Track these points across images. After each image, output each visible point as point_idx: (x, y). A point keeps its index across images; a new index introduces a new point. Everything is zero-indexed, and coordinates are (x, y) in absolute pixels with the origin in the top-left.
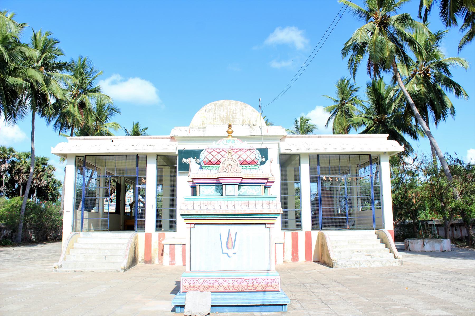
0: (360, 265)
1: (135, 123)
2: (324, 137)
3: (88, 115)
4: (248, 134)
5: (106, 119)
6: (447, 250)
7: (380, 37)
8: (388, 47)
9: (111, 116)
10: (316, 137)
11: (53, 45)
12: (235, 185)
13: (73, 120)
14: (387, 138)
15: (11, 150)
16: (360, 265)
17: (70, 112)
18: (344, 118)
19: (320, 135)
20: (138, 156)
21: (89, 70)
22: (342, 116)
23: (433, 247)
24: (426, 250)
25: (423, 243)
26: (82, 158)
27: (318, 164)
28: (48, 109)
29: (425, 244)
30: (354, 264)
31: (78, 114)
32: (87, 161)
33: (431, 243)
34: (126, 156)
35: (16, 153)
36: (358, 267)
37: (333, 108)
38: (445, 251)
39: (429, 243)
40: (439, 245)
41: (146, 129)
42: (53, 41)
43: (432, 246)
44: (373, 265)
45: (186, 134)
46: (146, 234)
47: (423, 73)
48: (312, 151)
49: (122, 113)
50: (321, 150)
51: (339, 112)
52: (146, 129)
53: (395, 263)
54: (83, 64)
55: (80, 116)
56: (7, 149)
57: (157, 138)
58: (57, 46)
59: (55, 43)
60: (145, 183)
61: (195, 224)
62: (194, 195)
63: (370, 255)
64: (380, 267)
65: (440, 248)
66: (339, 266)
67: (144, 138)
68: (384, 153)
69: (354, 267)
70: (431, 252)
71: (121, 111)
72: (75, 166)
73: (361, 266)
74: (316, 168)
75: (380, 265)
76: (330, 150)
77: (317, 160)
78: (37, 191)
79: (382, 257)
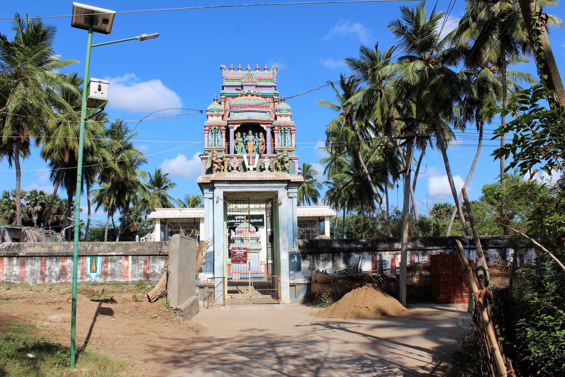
1: (157, 170)
3: (126, 171)
5: (135, 169)
7: (346, 128)
8: (351, 135)
9: (138, 166)
12: (295, 286)
13: (115, 174)
15: (42, 193)
17: (113, 168)
18: (337, 169)
21: (124, 131)
22: (335, 167)
31: (119, 169)
35: (46, 196)
37: (327, 160)
41: (167, 174)
47: (385, 145)
49: (148, 163)
51: (333, 164)
52: (167, 174)
54: (120, 125)
55: (120, 170)
56: (39, 193)
62: (290, 286)
71: (148, 161)
78: (451, 328)
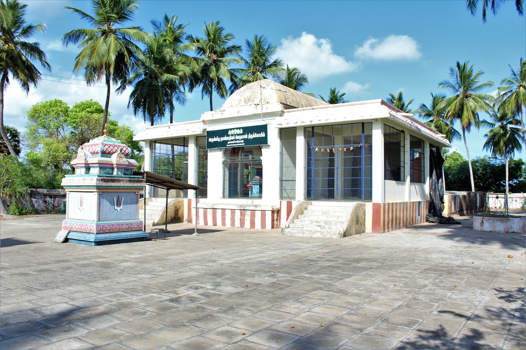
0: (303, 234)
2: (317, 108)
4: (251, 113)
6: (516, 231)
10: (310, 109)
11: (220, 33)
14: (380, 103)
16: (303, 234)
19: (313, 107)
20: (363, 123)
23: (493, 227)
24: (485, 230)
25: (482, 221)
26: (311, 129)
27: (363, 132)
28: (222, 91)
29: (484, 222)
30: (298, 233)
32: (315, 130)
33: (491, 221)
34: (352, 124)
36: (301, 235)
38: (514, 232)
39: (489, 221)
40: (503, 225)
41: (343, 95)
42: (219, 29)
43: (492, 225)
44: (315, 236)
45: (211, 118)
46: (374, 204)
48: (307, 123)
50: (315, 122)
52: (343, 95)
53: (334, 235)
57: (194, 123)
58: (224, 33)
59: (221, 31)
60: (187, 161)
61: (70, 191)
63: (320, 226)
64: (321, 238)
65: (505, 229)
66: (286, 233)
67: (342, 106)
68: (376, 120)
69: (297, 235)
70: (491, 232)
72: (305, 137)
73: (304, 235)
74: (361, 136)
75: (321, 236)
76: (323, 121)
77: (361, 127)
79: (331, 229)
